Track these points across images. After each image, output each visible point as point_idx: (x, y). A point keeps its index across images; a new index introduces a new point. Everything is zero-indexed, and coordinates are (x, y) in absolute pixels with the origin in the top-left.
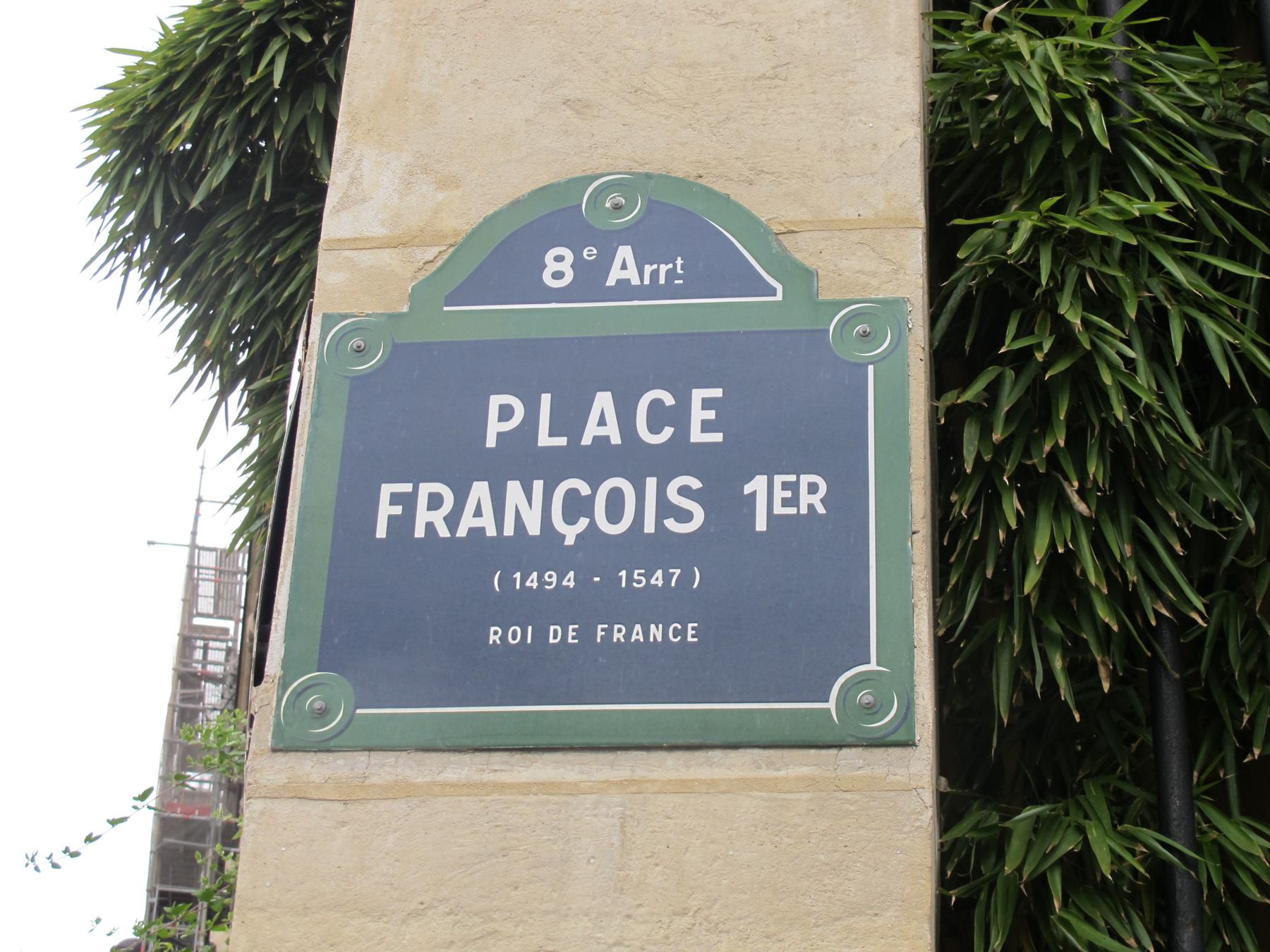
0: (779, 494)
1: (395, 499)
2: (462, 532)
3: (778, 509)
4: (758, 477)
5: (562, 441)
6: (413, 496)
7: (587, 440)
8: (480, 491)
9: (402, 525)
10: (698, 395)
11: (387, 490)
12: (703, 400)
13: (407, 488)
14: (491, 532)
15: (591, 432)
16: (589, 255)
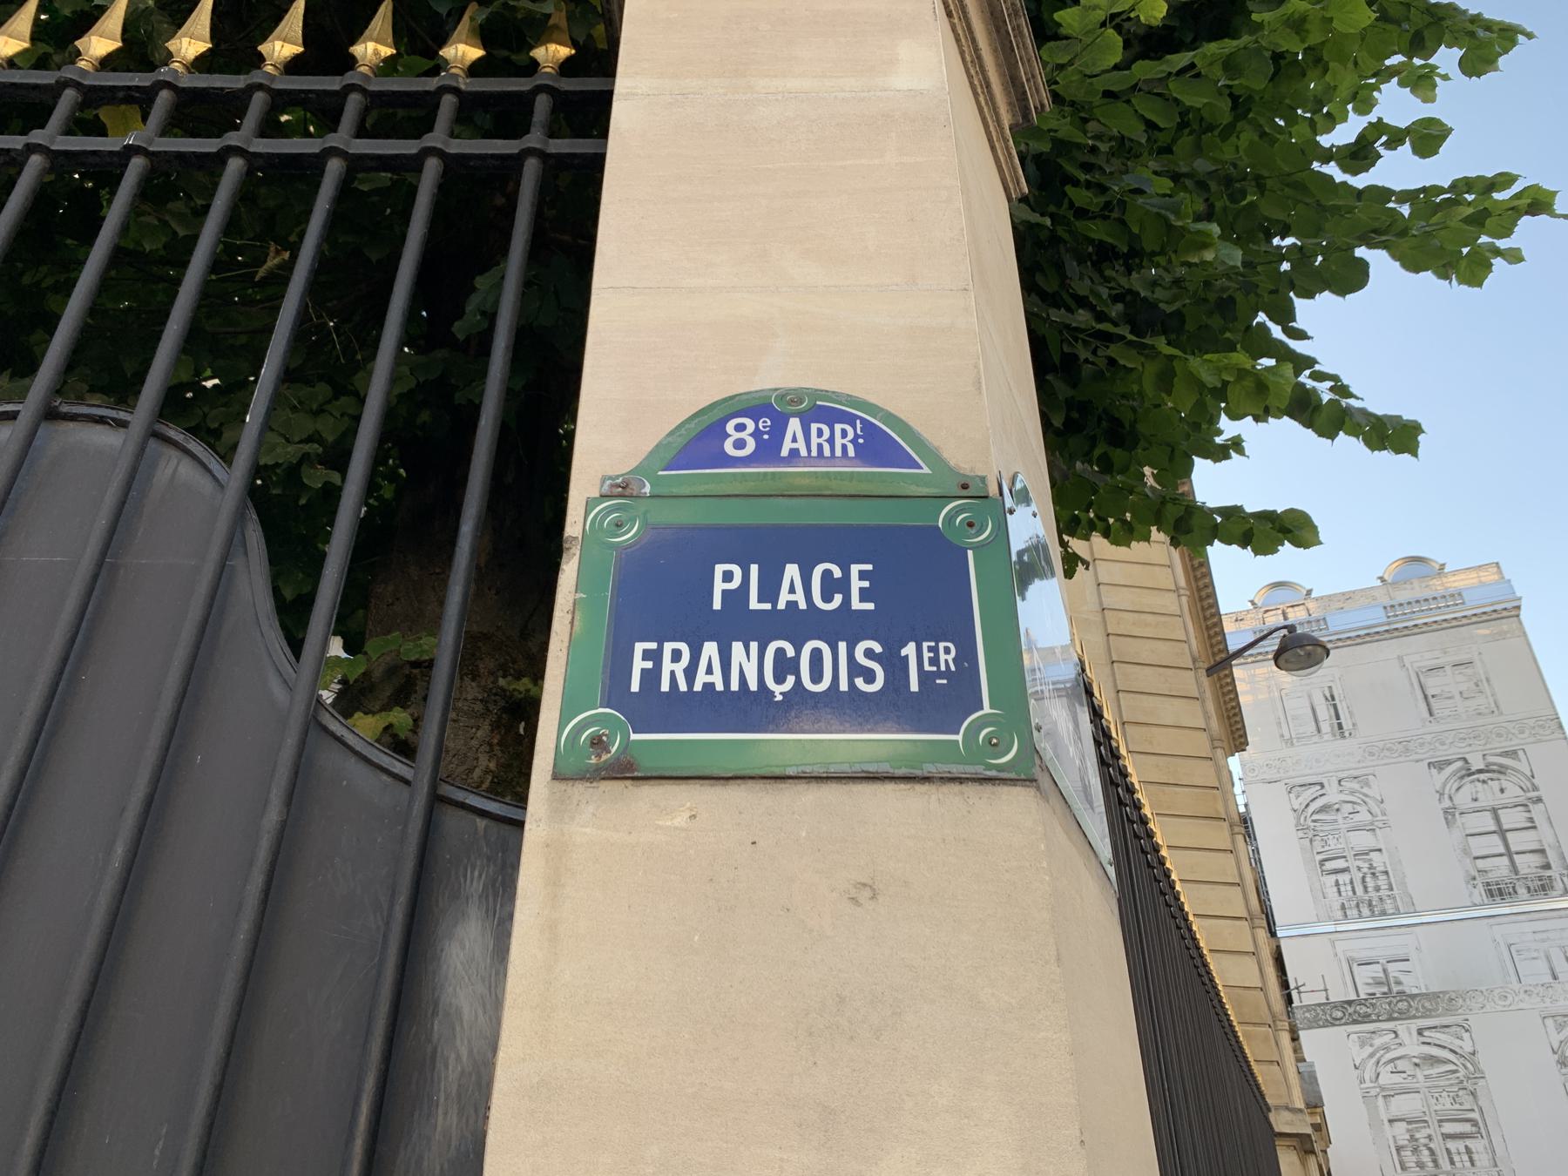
0: (927, 655)
1: (647, 655)
2: (698, 687)
3: (927, 667)
4: (910, 643)
5: (768, 606)
6: (660, 650)
7: (781, 605)
8: (710, 649)
9: (652, 677)
10: (855, 569)
11: (640, 647)
12: (860, 571)
13: (653, 645)
14: (720, 687)
15: (784, 598)
16: (764, 427)
